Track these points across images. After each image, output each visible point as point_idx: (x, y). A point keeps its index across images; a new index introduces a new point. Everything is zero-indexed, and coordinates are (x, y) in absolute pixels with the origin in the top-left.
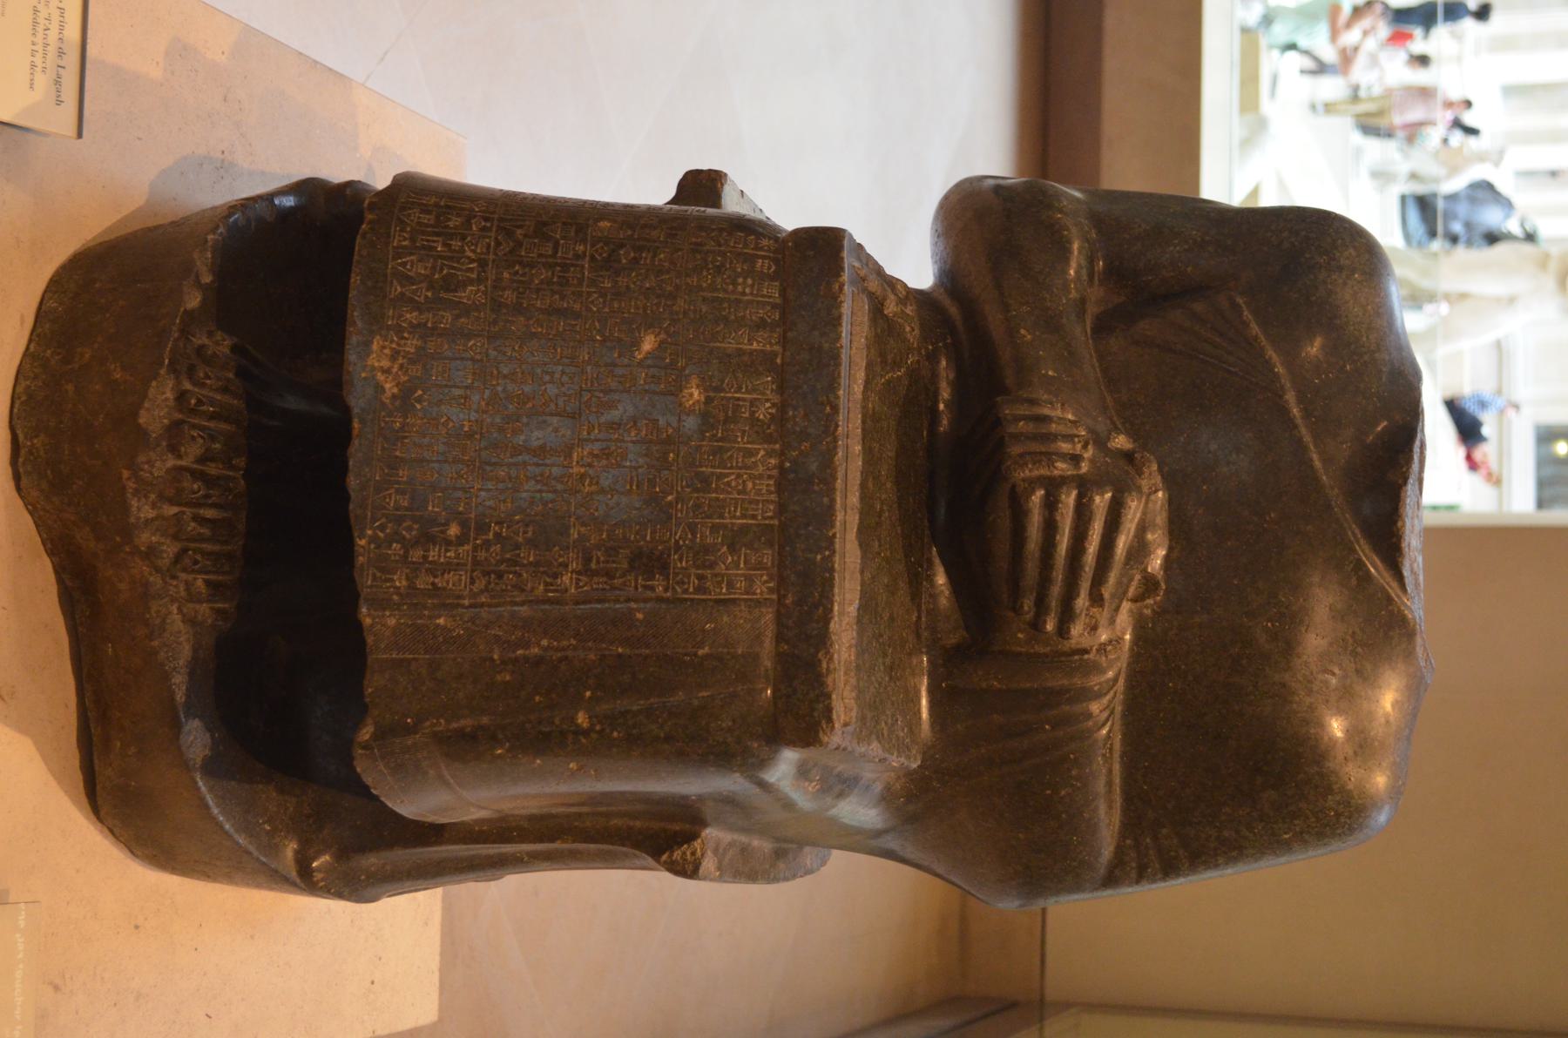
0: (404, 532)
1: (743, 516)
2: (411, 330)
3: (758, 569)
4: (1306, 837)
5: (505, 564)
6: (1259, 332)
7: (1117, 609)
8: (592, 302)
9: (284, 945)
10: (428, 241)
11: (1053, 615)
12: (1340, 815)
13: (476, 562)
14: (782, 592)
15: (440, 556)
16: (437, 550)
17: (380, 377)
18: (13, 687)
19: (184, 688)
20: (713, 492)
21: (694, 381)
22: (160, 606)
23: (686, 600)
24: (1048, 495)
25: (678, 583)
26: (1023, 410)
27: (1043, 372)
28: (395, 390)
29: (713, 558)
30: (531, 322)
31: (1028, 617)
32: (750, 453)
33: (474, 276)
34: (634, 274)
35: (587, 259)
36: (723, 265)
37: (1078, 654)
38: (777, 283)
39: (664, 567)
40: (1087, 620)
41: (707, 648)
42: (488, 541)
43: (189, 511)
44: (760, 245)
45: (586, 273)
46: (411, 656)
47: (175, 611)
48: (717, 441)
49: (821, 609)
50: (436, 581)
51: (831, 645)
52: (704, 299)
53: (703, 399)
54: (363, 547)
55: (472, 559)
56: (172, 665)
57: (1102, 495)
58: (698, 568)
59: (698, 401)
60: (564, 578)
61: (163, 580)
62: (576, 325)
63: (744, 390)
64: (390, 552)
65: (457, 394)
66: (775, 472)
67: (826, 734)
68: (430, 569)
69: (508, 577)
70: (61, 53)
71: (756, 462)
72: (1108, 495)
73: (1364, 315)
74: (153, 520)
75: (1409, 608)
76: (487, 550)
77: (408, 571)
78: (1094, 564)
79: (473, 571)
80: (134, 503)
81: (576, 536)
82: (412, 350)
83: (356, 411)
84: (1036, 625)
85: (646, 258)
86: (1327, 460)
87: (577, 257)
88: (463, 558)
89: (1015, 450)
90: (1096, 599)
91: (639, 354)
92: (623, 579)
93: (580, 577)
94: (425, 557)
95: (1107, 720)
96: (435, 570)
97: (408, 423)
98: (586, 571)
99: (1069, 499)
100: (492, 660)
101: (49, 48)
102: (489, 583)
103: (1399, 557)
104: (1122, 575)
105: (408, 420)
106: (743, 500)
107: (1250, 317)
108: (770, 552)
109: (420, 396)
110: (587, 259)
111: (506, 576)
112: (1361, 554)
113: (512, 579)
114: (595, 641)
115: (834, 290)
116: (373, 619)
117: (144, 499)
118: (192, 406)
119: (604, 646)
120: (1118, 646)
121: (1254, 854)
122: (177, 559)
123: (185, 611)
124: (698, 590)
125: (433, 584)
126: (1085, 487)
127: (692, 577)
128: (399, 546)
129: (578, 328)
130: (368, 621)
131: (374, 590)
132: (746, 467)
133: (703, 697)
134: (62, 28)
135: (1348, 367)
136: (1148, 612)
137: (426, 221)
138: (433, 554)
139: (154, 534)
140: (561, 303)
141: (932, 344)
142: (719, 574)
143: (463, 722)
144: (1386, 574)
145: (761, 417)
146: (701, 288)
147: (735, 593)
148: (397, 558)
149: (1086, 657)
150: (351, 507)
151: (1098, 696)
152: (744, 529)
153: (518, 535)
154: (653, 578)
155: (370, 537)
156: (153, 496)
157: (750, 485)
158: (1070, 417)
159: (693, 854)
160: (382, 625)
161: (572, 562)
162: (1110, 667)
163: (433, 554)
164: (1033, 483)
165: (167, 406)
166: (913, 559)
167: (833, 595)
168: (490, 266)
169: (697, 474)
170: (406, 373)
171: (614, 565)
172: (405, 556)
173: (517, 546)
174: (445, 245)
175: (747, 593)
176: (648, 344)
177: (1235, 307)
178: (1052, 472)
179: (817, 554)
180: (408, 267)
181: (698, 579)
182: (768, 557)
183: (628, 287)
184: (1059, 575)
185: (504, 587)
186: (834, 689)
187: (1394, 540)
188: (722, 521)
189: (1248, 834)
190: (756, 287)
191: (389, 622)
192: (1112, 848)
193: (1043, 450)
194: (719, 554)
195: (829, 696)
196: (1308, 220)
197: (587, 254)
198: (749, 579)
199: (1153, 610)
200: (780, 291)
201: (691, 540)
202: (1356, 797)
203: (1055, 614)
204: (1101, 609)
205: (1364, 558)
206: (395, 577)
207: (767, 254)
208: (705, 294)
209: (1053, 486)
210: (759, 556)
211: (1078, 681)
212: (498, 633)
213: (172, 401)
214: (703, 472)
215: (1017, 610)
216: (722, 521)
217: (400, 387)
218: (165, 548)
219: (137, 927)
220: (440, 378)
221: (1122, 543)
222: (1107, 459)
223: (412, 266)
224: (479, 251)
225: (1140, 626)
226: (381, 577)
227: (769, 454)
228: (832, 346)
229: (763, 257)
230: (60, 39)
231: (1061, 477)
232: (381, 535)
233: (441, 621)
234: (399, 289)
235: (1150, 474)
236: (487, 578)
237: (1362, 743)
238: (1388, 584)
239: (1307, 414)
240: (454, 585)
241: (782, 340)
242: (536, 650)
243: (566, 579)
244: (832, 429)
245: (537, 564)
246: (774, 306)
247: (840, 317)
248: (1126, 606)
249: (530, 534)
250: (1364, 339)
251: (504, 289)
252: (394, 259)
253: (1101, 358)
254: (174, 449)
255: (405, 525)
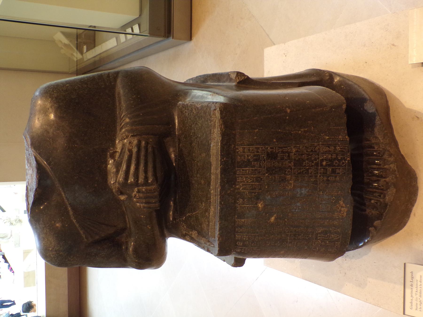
0: (337, 162)
1: (246, 170)
2: (336, 219)
3: (241, 155)
4: (62, 85)
5: (311, 154)
6: (80, 231)
7: (122, 149)
8: (288, 230)
9: (316, 63)
10: (331, 244)
11: (143, 146)
12: (52, 91)
13: (318, 154)
14: (235, 148)
15: (328, 156)
16: (329, 158)
17: (344, 205)
18: (413, 120)
19: (376, 120)
20: (255, 177)
21: (260, 209)
22: (386, 141)
23: (262, 145)
24: (147, 181)
25: (264, 150)
26: (152, 205)
27: (145, 217)
28: (340, 202)
29: (255, 158)
30: (304, 223)
31: (149, 145)
32: (244, 189)
33: (319, 235)
34: (276, 239)
35: (288, 242)
36: (252, 243)
37: (135, 135)
38: (236, 239)
39: (268, 154)
40: (132, 145)
41: (256, 131)
42: (315, 161)
43: (381, 167)
44: (240, 250)
45: (289, 238)
46: (335, 127)
47: (381, 140)
48: (254, 192)
49: (224, 143)
50: (328, 149)
51: (221, 133)
52: (257, 233)
53: (258, 204)
54: (349, 158)
55: (319, 155)
56: (381, 126)
57: (131, 182)
58: (259, 154)
59: (259, 203)
60: (295, 150)
61: (386, 148)
62: (292, 223)
63: (246, 207)
64: (341, 156)
65: (324, 202)
66: (237, 183)
67: (221, 107)
68: (330, 152)
69: (310, 150)
70: (412, 285)
71: (243, 186)
72: (129, 181)
73: (48, 238)
74: (391, 164)
75: (34, 152)
76: (315, 158)
77: (336, 151)
78: (132, 161)
79: (319, 152)
80: (395, 168)
81: (292, 163)
82: (335, 213)
83: (350, 196)
84: (147, 143)
85: (273, 243)
86: (60, 194)
87: (291, 242)
88: (322, 155)
89: (156, 193)
90: (130, 151)
91: (275, 216)
92: (279, 151)
93: (291, 151)
94: (332, 155)
95: (123, 117)
96: (329, 152)
97: (337, 193)
98: (289, 153)
99: (141, 180)
100: (313, 127)
101: (416, 286)
102: (315, 149)
103: (37, 167)
104: (123, 159)
105: (337, 193)
106: (246, 175)
107: (83, 235)
108: (238, 160)
109: (333, 201)
110: (288, 242)
111: (310, 151)
112: (49, 167)
113: (309, 150)
114: (287, 133)
115: (221, 238)
116: (345, 138)
117: (393, 169)
118: (382, 195)
119: (284, 131)
120: (122, 138)
121: (76, 80)
122: (384, 154)
123: (379, 140)
124: (258, 148)
125: (329, 148)
126: (136, 184)
127: (260, 152)
128: (339, 158)
129: (291, 222)
130: (347, 137)
131: (345, 146)
132: (245, 185)
133: (256, 117)
134: (412, 292)
135: (53, 222)
136: (111, 149)
137: (330, 249)
138: (330, 156)
139: (390, 160)
140: (296, 229)
141: (174, 223)
142: (253, 153)
143: (319, 109)
144: (41, 161)
145: (241, 200)
146: (258, 236)
147: (248, 148)
148: (339, 155)
149: (132, 134)
150: (351, 169)
151: (127, 123)
152: (246, 166)
153: (307, 163)
154: (271, 151)
155: (346, 160)
156: (391, 170)
157: (244, 179)
158: (138, 204)
159: (239, 78)
160: (343, 136)
161: (293, 155)
162: (124, 132)
163: (330, 156)
164: (151, 184)
165: (388, 194)
166: (182, 161)
167: (221, 148)
168: (314, 238)
169: (260, 182)
170: (337, 207)
171: (282, 155)
172: (337, 155)
173: (307, 159)
174: (326, 243)
175: (245, 147)
176: (273, 219)
177: (87, 238)
178: (146, 188)
179: (225, 160)
180: (336, 236)
181: (259, 152)
182: (239, 159)
183: (278, 235)
184: (142, 157)
185: (311, 148)
186: (220, 120)
187: (39, 172)
188: (252, 169)
189: (79, 86)
190: (243, 237)
191: (341, 137)
192: (118, 82)
193: (148, 194)
194: (253, 159)
195: (221, 118)
196: (65, 264)
197: (288, 243)
198: (244, 152)
199: (110, 149)
200: (236, 237)
201: (261, 163)
202: (48, 96)
203: (142, 147)
204: (129, 148)
205: (48, 166)
206: (340, 149)
207: (239, 247)
208: (257, 234)
209: (146, 183)
210: (241, 158)
211: (134, 128)
212: (312, 134)
213: (386, 196)
214: (258, 183)
215: (153, 148)
216: (252, 169)
217: (339, 203)
218: (387, 157)
219: (366, 63)
220: (328, 206)
221: (124, 167)
222: (128, 192)
223: (335, 236)
224: (317, 242)
225: (114, 145)
226: (343, 149)
227: (239, 189)
228: (222, 222)
229: (240, 246)
230: (412, 289)
231: (143, 186)
232: (343, 161)
233: (327, 137)
234: (339, 230)
235: (115, 188)
236: (315, 150)
237: (45, 112)
238: (40, 159)
239: (66, 208)
240: (324, 148)
241: (235, 222)
242: (302, 130)
243: (294, 150)
244: (221, 197)
245: (302, 155)
246: (237, 232)
247: (219, 230)
248: (119, 150)
249: (304, 163)
250: (48, 231)
251: (311, 232)
252: (339, 239)
253: (125, 221)
254: (387, 183)
255: (337, 164)
